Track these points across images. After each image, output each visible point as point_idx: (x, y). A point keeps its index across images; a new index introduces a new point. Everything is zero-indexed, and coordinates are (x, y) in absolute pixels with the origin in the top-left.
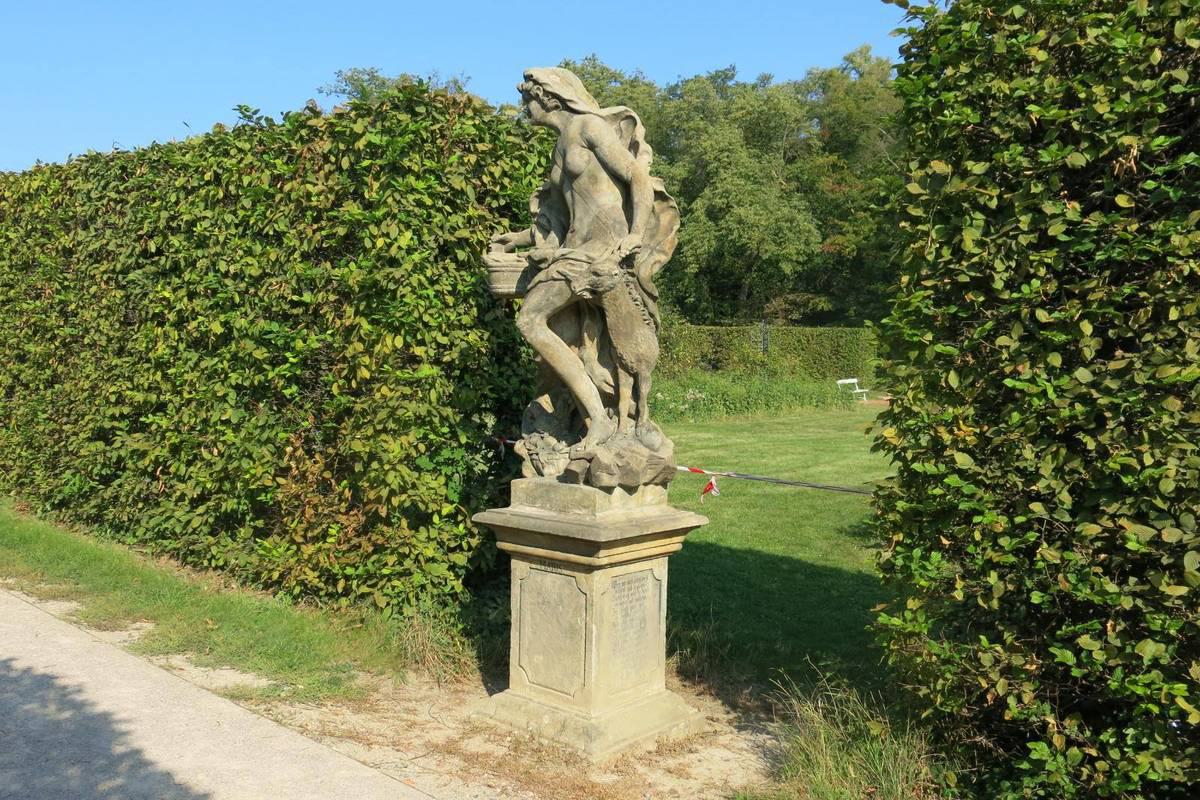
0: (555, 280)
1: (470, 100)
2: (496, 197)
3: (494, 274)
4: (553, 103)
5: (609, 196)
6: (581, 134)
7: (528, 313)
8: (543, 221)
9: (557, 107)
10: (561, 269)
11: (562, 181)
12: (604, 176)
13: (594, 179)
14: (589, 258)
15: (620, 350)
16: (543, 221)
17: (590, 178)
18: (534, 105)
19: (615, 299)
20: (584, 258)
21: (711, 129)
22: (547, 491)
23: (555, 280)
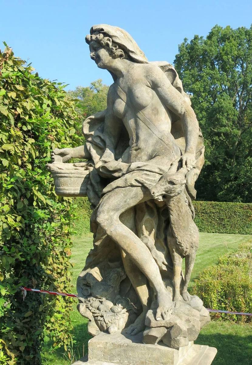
0: (132, 186)
1: (12, 54)
2: (24, 123)
3: (62, 180)
4: (119, 52)
5: (165, 123)
6: (146, 77)
7: (108, 212)
8: (98, 141)
9: (121, 56)
10: (138, 178)
11: (126, 111)
12: (163, 110)
13: (156, 111)
14: (161, 170)
15: (179, 239)
16: (98, 141)
17: (153, 110)
18: (103, 53)
19: (179, 202)
20: (157, 171)
21: (217, 85)
22: (125, 350)
23: (132, 186)
